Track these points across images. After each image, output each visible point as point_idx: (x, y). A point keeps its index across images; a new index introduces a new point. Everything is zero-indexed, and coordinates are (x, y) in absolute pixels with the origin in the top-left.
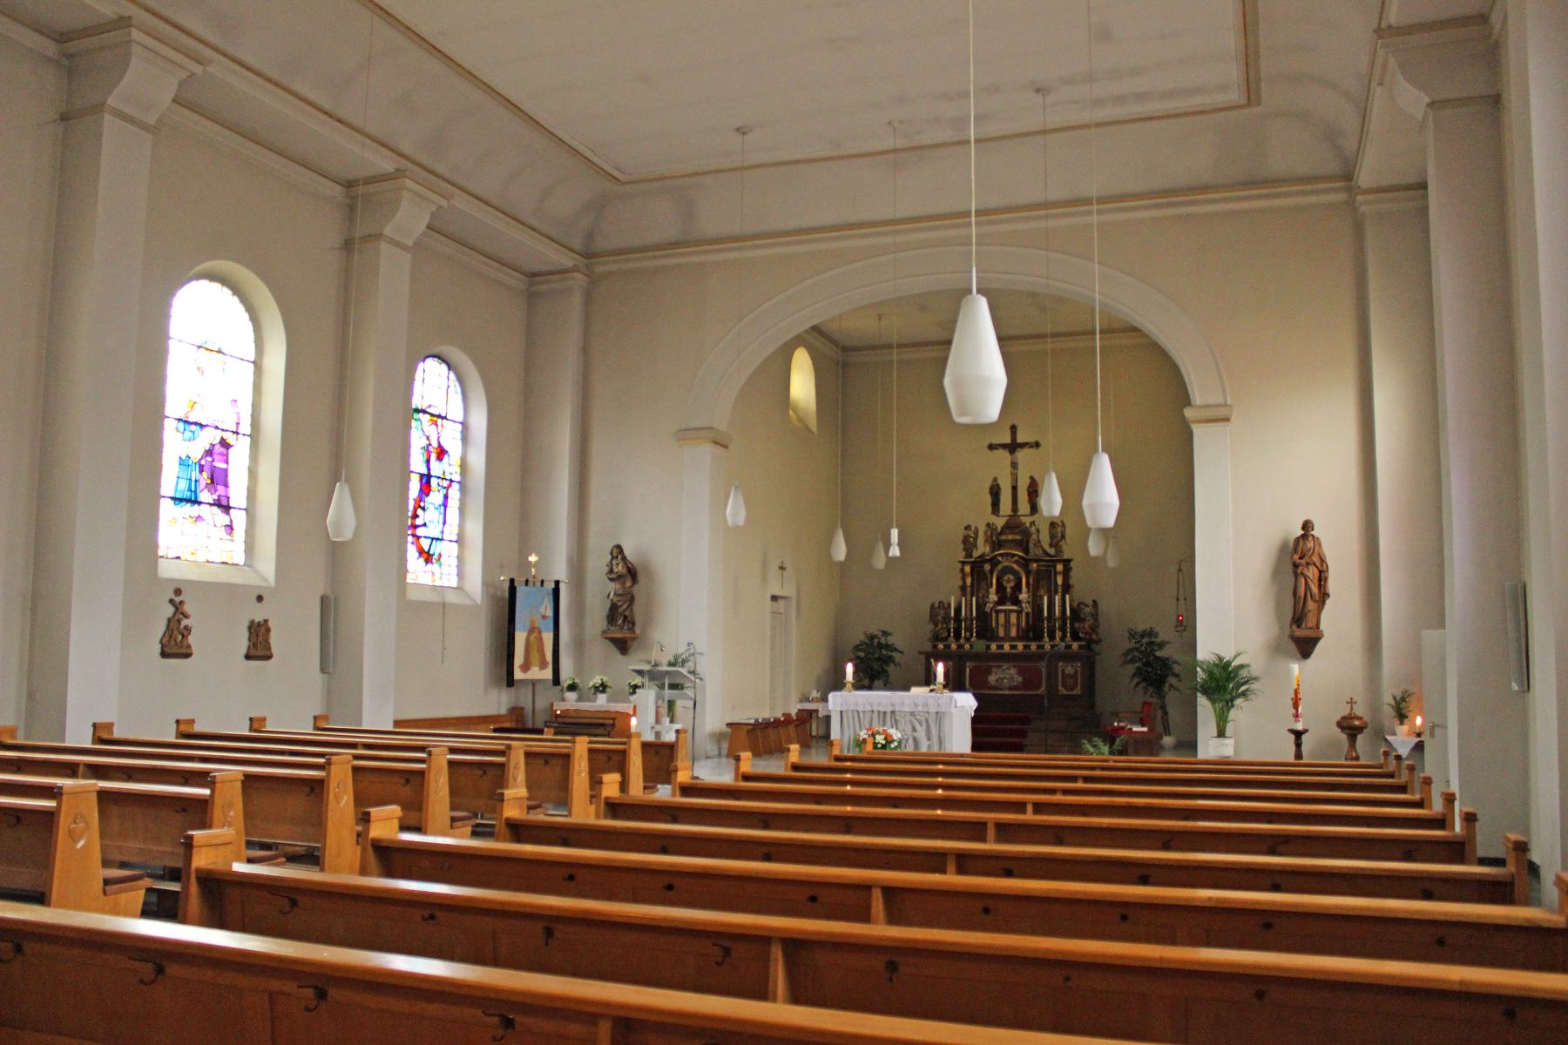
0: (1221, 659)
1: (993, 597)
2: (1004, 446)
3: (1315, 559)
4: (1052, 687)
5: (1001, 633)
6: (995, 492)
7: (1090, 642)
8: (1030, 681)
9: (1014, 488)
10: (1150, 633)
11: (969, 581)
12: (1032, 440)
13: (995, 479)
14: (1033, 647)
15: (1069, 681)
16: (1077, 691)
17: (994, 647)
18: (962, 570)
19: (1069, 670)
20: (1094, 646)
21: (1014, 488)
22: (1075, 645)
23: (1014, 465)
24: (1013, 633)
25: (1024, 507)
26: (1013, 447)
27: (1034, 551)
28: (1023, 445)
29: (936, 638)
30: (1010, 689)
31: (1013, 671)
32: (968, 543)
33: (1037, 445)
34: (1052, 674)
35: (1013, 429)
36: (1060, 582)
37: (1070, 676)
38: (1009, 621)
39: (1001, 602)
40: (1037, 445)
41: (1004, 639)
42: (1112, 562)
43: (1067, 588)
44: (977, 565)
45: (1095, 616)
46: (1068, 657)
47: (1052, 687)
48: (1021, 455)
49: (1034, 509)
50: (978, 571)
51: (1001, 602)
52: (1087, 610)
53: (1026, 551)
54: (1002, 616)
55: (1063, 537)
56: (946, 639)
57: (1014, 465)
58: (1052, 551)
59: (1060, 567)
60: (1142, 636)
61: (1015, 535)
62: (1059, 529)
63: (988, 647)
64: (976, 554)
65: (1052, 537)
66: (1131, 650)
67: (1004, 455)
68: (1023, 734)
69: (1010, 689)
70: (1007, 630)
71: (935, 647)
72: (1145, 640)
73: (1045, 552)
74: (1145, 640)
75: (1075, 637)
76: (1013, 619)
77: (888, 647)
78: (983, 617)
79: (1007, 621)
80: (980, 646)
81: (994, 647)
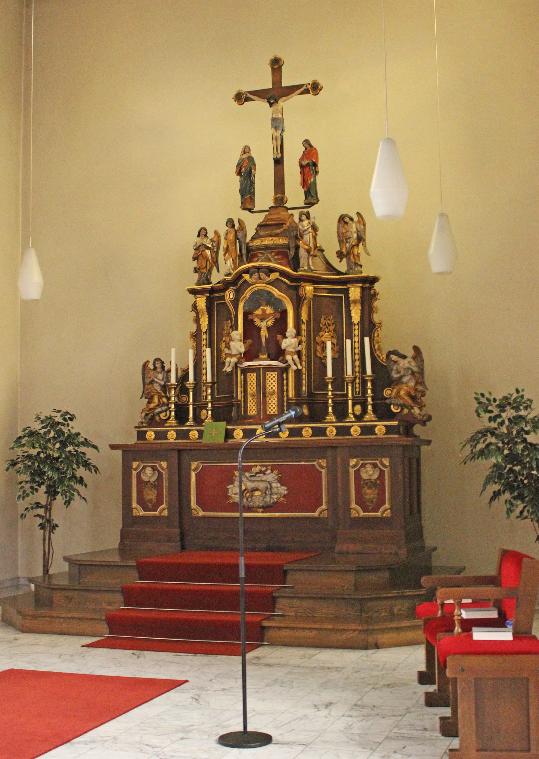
0: (378, 294)
1: (238, 346)
2: (260, 94)
3: (240, 421)
4: (339, 505)
5: (252, 411)
6: (246, 171)
7: (407, 427)
8: (302, 488)
9: (279, 162)
10: (517, 402)
11: (205, 322)
12: (307, 80)
13: (246, 150)
14: (307, 431)
15: (370, 494)
16: (385, 511)
17: (238, 433)
18: (195, 307)
19: (369, 473)
20: (417, 429)
21: (279, 162)
22: (380, 427)
23: (277, 124)
24: (272, 408)
25: (295, 195)
26: (275, 94)
27: (310, 265)
28: (291, 90)
29: (151, 420)
30: (266, 508)
31: (271, 477)
32: (204, 257)
33: (315, 88)
34: (337, 475)
35: (276, 64)
36: (356, 316)
37: (371, 484)
38: (267, 392)
39: (249, 355)
40: (315, 88)
41: (256, 420)
42: (437, 261)
43: (369, 327)
44: (214, 296)
45: (419, 375)
46: (367, 449)
47: (339, 505)
48: (290, 105)
49: (311, 195)
50: (214, 301)
51: (249, 355)
52: (403, 363)
53: (295, 263)
54: (252, 377)
55: (360, 239)
56: (163, 423)
57: (277, 124)
58: (342, 266)
59: (355, 292)
60: (502, 407)
61: (276, 245)
62: (353, 227)
63: (229, 435)
64: (216, 278)
65: (342, 239)
66: (484, 433)
67: (260, 106)
68: (268, 603)
69: (266, 508)
70: (262, 405)
71: (141, 435)
72: (510, 413)
73: (330, 267)
74: (510, 413)
75: (383, 412)
76: (272, 380)
77: (72, 439)
78: (224, 382)
79: (261, 385)
80: (214, 431)
81: (238, 433)
